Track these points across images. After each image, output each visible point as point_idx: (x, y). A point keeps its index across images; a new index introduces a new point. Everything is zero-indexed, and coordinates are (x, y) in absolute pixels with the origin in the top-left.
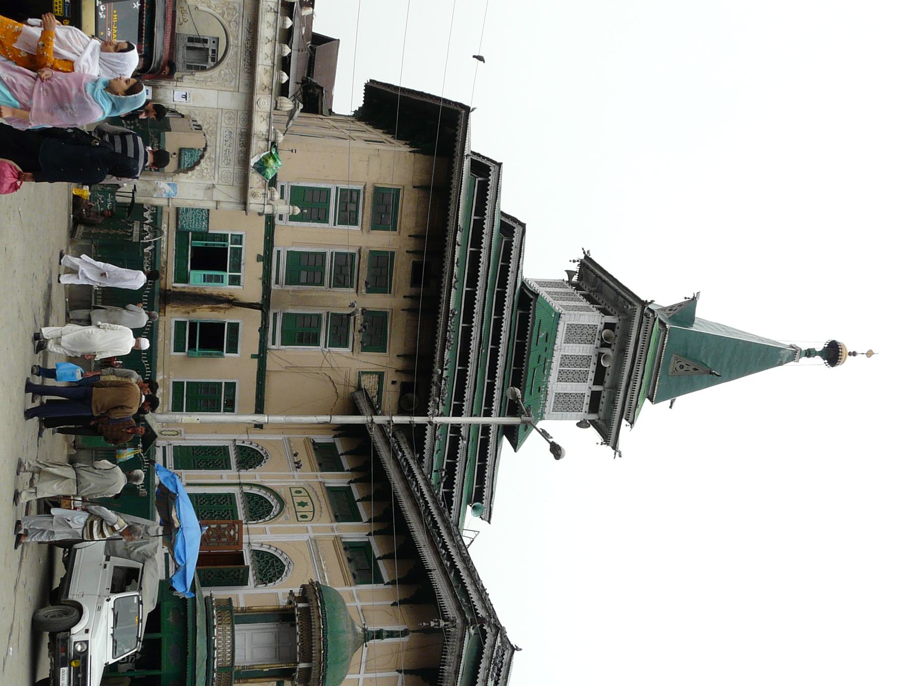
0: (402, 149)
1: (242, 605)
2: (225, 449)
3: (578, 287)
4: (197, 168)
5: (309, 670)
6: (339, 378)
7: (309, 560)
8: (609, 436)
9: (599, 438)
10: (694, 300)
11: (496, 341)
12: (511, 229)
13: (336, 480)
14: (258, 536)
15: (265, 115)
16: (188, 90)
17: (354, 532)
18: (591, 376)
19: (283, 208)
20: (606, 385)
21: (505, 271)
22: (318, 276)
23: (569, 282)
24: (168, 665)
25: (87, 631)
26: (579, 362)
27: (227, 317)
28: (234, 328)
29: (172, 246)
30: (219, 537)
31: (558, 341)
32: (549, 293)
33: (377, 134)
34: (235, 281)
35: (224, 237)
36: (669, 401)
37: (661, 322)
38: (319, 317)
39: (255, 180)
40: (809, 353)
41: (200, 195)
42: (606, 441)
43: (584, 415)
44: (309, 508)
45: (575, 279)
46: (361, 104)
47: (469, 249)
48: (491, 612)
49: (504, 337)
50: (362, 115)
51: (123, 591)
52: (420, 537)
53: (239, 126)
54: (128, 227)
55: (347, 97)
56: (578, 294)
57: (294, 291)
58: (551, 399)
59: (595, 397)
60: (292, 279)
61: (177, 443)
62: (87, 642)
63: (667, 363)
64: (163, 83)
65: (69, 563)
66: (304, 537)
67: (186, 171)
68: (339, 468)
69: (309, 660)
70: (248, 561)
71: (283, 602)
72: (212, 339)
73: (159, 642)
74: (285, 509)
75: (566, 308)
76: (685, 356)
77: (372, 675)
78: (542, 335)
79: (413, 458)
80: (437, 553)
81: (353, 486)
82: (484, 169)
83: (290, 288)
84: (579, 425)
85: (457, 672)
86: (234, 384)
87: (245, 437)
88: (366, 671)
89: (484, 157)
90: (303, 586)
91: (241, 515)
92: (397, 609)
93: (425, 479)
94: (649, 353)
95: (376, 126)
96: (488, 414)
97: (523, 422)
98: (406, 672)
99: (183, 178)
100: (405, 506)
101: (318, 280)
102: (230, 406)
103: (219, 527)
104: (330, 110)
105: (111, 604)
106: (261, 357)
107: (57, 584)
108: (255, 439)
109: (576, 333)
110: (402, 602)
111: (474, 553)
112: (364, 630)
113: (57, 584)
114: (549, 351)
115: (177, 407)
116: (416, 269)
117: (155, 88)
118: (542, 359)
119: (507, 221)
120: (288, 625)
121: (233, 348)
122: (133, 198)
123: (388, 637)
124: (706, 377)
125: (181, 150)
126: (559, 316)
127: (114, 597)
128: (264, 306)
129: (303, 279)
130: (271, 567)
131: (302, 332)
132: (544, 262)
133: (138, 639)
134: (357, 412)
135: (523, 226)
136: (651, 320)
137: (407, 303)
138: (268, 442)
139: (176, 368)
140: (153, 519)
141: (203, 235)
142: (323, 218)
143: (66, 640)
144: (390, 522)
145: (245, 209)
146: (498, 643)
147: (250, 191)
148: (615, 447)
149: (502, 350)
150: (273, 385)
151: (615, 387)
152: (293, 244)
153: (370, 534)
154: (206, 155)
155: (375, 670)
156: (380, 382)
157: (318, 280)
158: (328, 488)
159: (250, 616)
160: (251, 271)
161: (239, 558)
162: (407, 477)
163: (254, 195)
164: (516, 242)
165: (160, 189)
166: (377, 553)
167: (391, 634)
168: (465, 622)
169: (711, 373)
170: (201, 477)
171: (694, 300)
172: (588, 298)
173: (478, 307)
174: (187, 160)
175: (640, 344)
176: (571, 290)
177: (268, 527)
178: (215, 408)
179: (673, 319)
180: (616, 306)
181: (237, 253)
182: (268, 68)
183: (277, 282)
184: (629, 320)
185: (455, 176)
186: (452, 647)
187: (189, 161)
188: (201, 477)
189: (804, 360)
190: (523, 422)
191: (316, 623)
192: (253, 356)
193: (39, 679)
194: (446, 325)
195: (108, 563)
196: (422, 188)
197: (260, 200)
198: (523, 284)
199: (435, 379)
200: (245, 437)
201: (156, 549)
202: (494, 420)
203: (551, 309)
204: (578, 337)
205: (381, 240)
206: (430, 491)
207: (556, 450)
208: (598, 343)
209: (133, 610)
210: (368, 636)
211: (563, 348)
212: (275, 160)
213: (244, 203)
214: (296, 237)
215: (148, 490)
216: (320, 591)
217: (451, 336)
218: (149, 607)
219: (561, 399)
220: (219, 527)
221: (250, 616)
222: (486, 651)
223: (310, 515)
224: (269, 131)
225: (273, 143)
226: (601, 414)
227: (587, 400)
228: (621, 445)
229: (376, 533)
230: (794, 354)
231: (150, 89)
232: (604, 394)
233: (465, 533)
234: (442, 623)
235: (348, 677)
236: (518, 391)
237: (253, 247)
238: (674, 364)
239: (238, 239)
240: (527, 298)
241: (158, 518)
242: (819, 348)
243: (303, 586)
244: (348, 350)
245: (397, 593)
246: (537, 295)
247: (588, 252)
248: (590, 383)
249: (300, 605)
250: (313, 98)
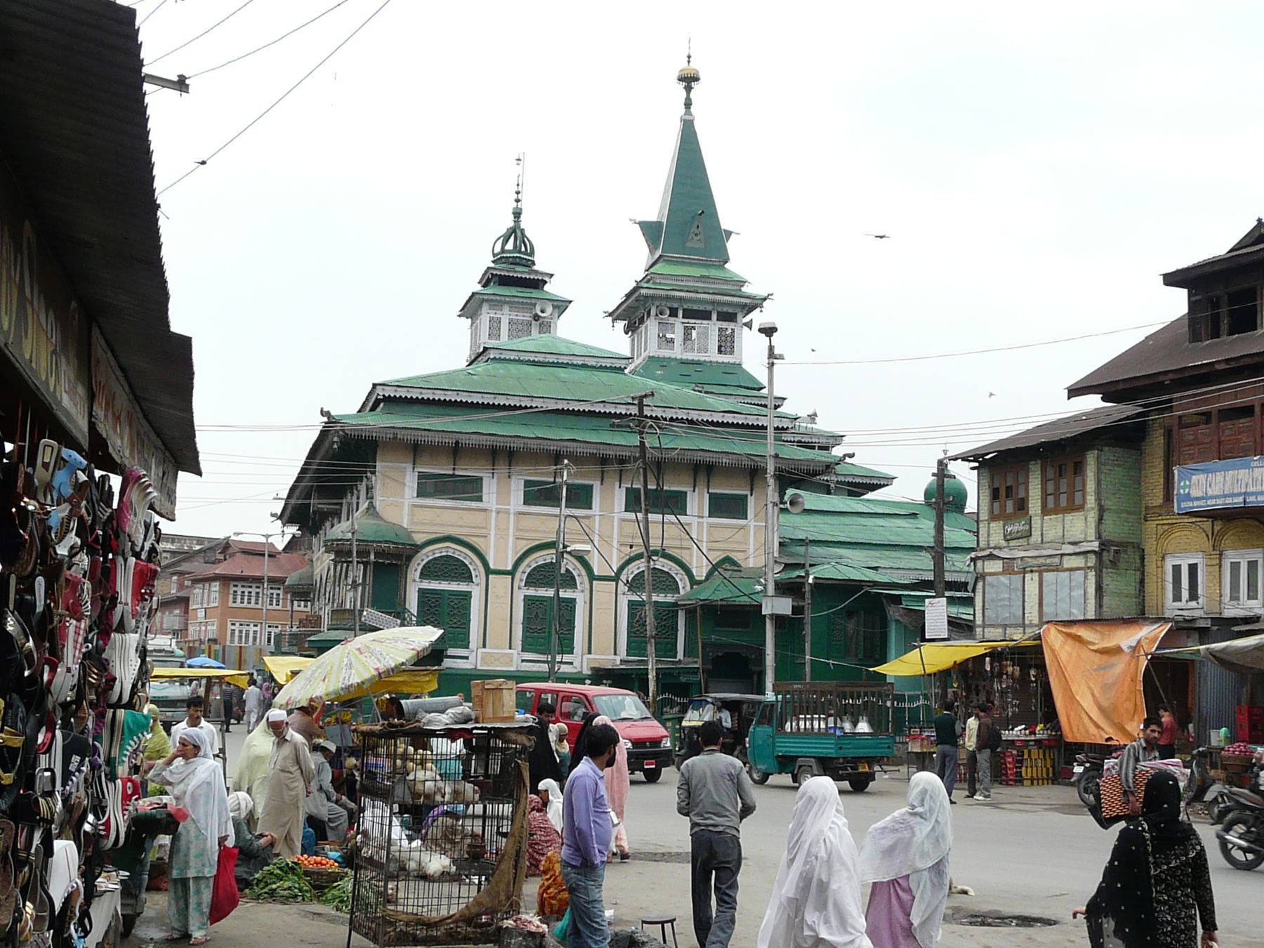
8: (755, 304)
59: (723, 317)
227: (724, 325)
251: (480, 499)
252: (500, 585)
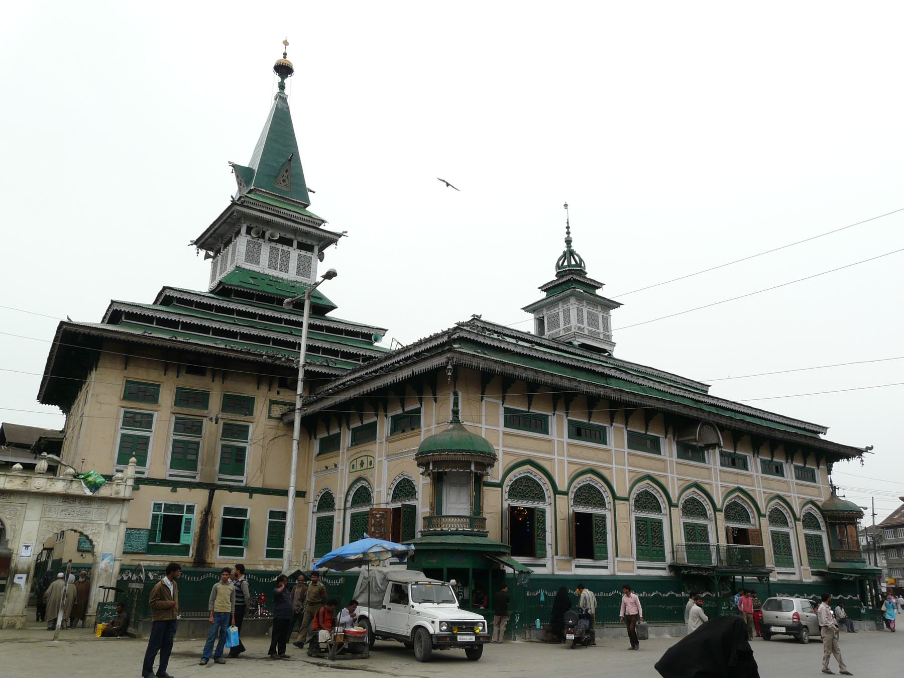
0: (94, 376)
1: (428, 510)
2: (319, 519)
3: (218, 252)
4: (90, 537)
5: (477, 464)
6: (272, 433)
7: (398, 461)
8: (331, 239)
9: (332, 246)
10: (234, 166)
11: (254, 315)
12: (167, 298)
13: (346, 439)
14: (382, 497)
15: (49, 483)
16: (21, 545)
17: (384, 427)
18: (285, 248)
19: (131, 470)
20: (293, 237)
21: (200, 305)
22: (190, 446)
23: (213, 258)
24: (466, 564)
25: (433, 622)
26: (274, 256)
27: (219, 515)
28: (227, 511)
29: (158, 557)
30: (381, 525)
31: (257, 270)
32: (221, 273)
33: (81, 396)
34: (190, 509)
35: (155, 517)
36: (309, 193)
37: (249, 193)
38: (223, 446)
39: (105, 492)
40: (282, 87)
41: (114, 535)
42: (334, 241)
43: (314, 256)
44: (365, 459)
45: (212, 254)
46: (57, 407)
47: (179, 330)
48: (444, 333)
49: (251, 310)
50: (66, 408)
51: (407, 595)
52: (389, 380)
53: (57, 504)
54: (132, 592)
55: (51, 419)
56: (223, 252)
57: (202, 465)
58: (300, 279)
59: (301, 246)
60: (193, 466)
61: (312, 555)
62: (441, 622)
63: (280, 191)
64: (13, 565)
65: (387, 636)
66: (385, 463)
67: (93, 547)
68: (337, 437)
69: (470, 463)
70: (398, 505)
71: (428, 480)
72: (235, 528)
73: (449, 570)
74: (364, 476)
75: (232, 262)
76: (276, 177)
77: (484, 417)
78: (252, 281)
79: (335, 381)
80: (401, 368)
81: (352, 426)
82: (116, 314)
83: (199, 467)
84: (321, 261)
85: (485, 359)
86: (271, 512)
87: (311, 505)
88: (480, 422)
89: (106, 314)
90: (418, 465)
91: (366, 509)
92: (128, 368)
93: (350, 374)
94: (271, 203)
95: (75, 397)
96: (300, 324)
97: (309, 298)
98: (483, 393)
99: (98, 549)
100: (368, 390)
101: (194, 446)
102: (284, 515)
103: (374, 525)
104: (61, 432)
105: (416, 605)
106: (251, 491)
107: (402, 645)
108: (313, 497)
109: (253, 256)
110: (434, 394)
111: (408, 341)
112: (451, 423)
113: (402, 645)
114: (264, 277)
115: (280, 554)
116: (192, 371)
117: (16, 572)
118: (270, 283)
119: (160, 300)
120: (445, 477)
121: (243, 512)
122: (109, 588)
123: (457, 406)
124: (293, 164)
125: (79, 550)
126: (238, 267)
127: (411, 603)
128: (212, 488)
129: (193, 457)
130: (404, 488)
131: (234, 460)
132: (197, 275)
133: (443, 585)
134: (291, 424)
135: (165, 288)
136: (247, 199)
137: (218, 381)
138: (316, 487)
139: (254, 556)
140: (359, 573)
141: (152, 533)
142: (145, 441)
143: (438, 637)
144: (378, 401)
145: (129, 500)
146: (468, 328)
147: (113, 496)
148: (340, 236)
149: (260, 312)
150: (273, 482)
151: (295, 231)
152: (164, 463)
153: (386, 416)
154: (80, 530)
155: (481, 416)
156: (277, 403)
157: (194, 446)
158: (352, 445)
159: (437, 504)
160: (184, 497)
161: (396, 511)
162: (347, 388)
163: (117, 493)
164: (175, 295)
165: (106, 567)
166: (399, 411)
167: (456, 404)
168: (450, 350)
169: (290, 160)
170: (338, 537)
171: (234, 166)
172: (227, 245)
173: (225, 327)
174: (87, 546)
175: (264, 209)
176: (219, 257)
177: (376, 490)
178: (283, 525)
179: (248, 183)
180: (234, 224)
181: (168, 507)
182: (8, 479)
183: (194, 477)
184: (246, 217)
185: (118, 336)
186: (466, 360)
187: (86, 545)
188: (338, 537)
189: (286, 91)
190: (309, 298)
191: (444, 457)
192: (251, 497)
193: (466, 656)
194: (237, 351)
195: (388, 607)
196: (126, 363)
197: (122, 488)
198: (211, 292)
199: (269, 361)
200: (311, 505)
201: (380, 572)
202: (305, 320)
203: (233, 273)
204: (255, 255)
205: (167, 397)
206: (358, 371)
207: (330, 275)
208: (261, 241)
209: (423, 588)
210: (456, 420)
211: (263, 266)
212: (89, 476)
213: (124, 501)
214: (159, 461)
215: (340, 577)
216: (421, 453)
217: (245, 348)
218: (421, 577)
219: (301, 271)
220: (374, 525)
221: (437, 504)
222: (472, 337)
223: (370, 459)
224: (64, 480)
225: (75, 477)
226: (314, 243)
227: (303, 253)
228: (339, 231)
229: (386, 411)
230: (281, 98)
231: (17, 576)
232: (300, 239)
233: (393, 348)
234: (450, 367)
235: (483, 436)
236: (286, 301)
237: (165, 496)
238: (281, 186)
239: (157, 506)
240: (222, 290)
241: (356, 569)
242: (279, 79)
243: (418, 465)
244: (251, 426)
245: (428, 397)
246: (221, 283)
248: (290, 249)
249: (431, 468)
250: (50, 444)
251: (703, 461)
252: (621, 507)
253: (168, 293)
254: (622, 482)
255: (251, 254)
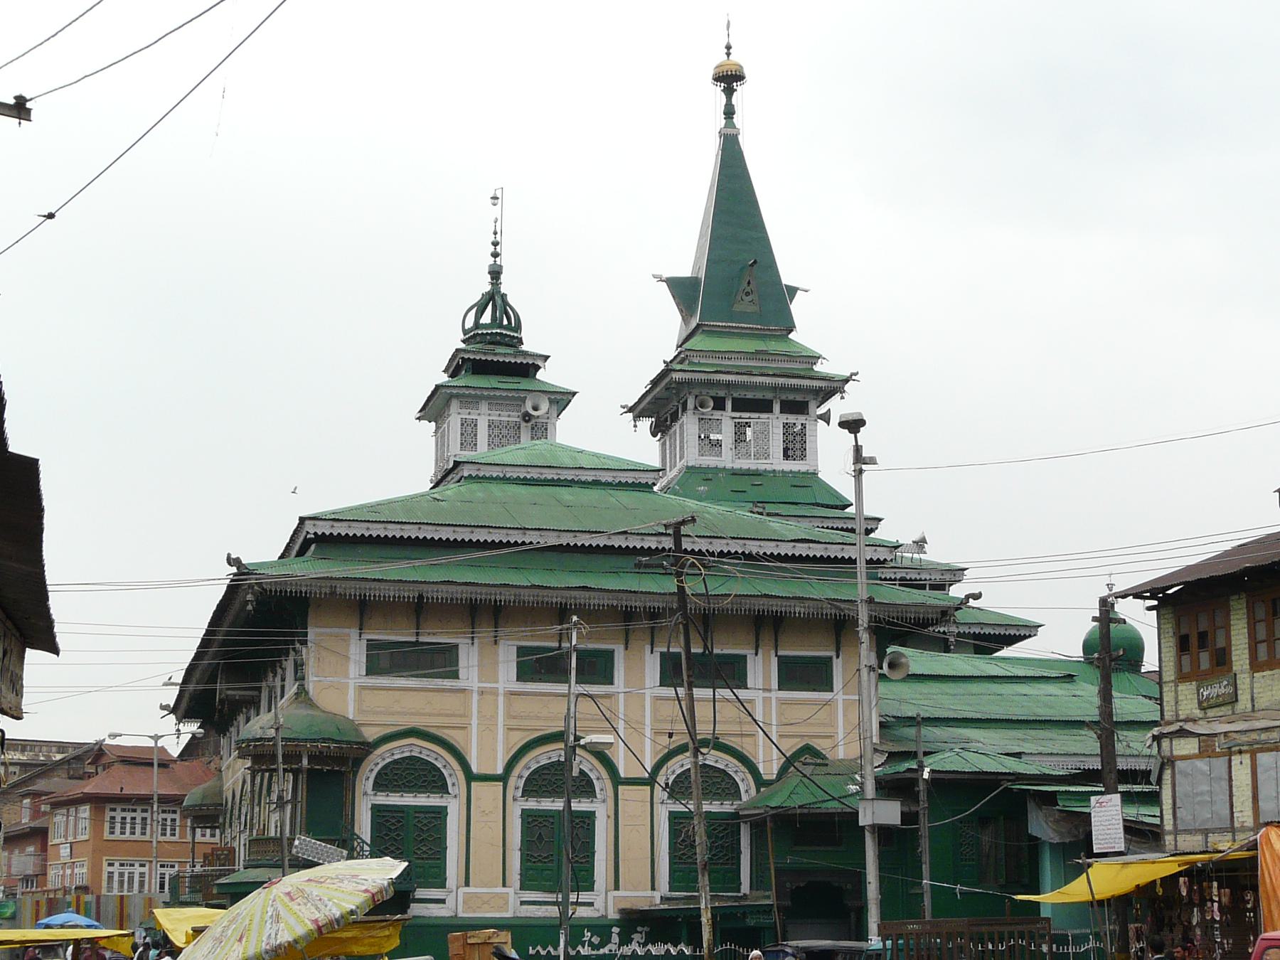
40: (729, 112)
59: (740, 405)
98: (418, 618)
148: (847, 381)
176: (667, 438)
189: (737, 119)
227: (791, 419)
247: (623, 407)
251: (455, 675)
252: (487, 794)
253: (310, 528)
254: (488, 747)
255: (496, 431)
